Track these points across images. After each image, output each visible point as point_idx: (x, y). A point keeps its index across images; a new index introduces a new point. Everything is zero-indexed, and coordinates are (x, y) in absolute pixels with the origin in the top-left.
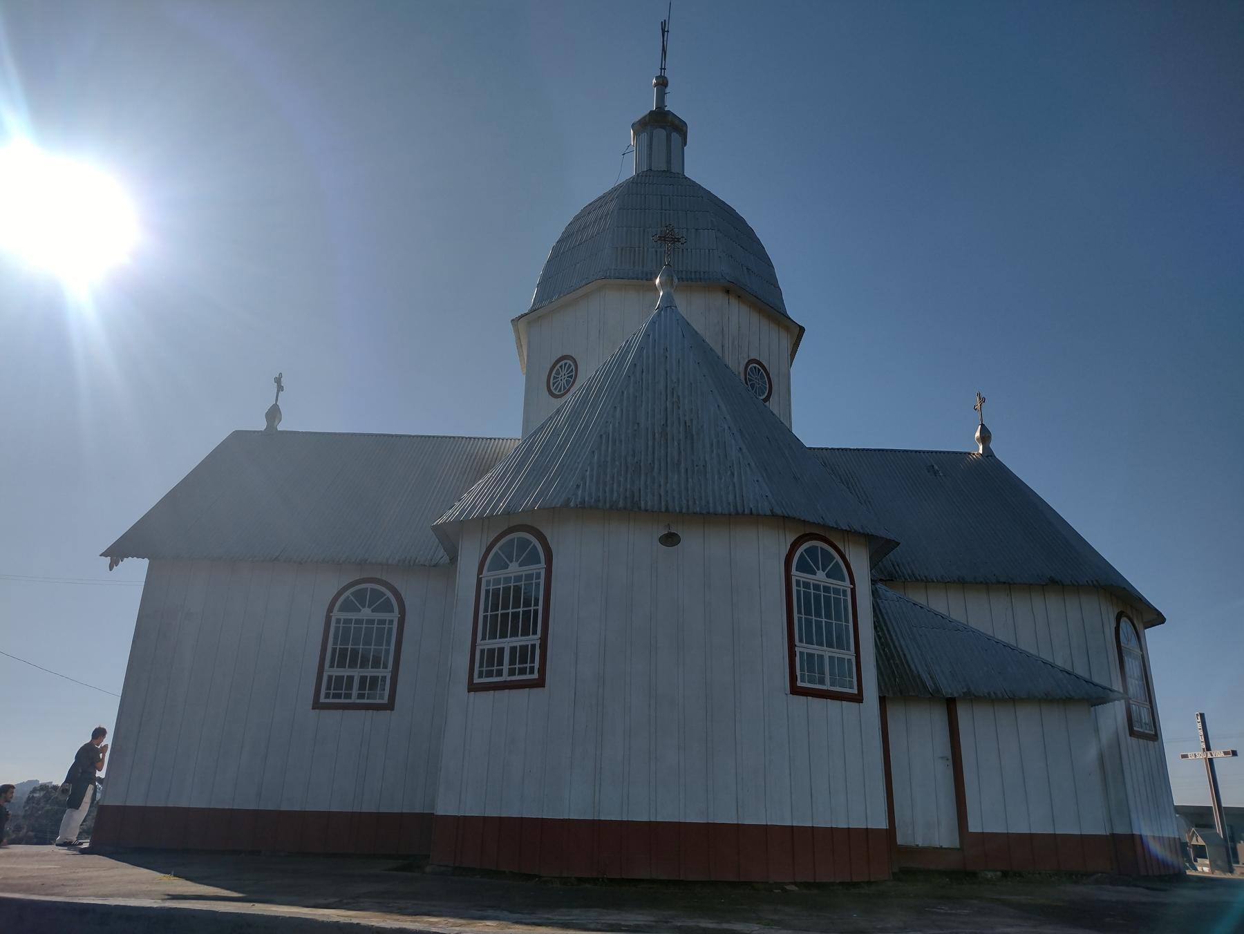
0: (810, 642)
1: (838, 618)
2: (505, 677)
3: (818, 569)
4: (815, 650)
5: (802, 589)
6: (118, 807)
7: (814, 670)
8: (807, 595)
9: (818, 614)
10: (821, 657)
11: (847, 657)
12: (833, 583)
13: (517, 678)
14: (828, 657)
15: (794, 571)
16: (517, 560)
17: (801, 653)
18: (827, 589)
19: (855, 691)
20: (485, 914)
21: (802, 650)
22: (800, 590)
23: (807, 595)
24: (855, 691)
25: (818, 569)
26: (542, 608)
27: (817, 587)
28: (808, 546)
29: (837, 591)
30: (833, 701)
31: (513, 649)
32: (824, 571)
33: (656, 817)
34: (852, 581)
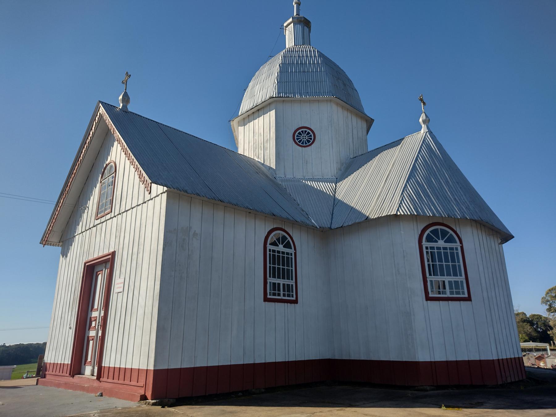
0: (274, 277)
1: (288, 266)
2: (281, 297)
3: (280, 244)
4: (276, 281)
5: (272, 253)
6: (318, 360)
7: (460, 288)
8: (274, 256)
9: (448, 266)
10: (279, 284)
11: (291, 284)
12: (286, 250)
13: (455, 296)
14: (447, 282)
15: (268, 245)
16: (280, 244)
17: (431, 281)
18: (283, 253)
19: (466, 295)
20: (358, 404)
21: (270, 281)
22: (271, 254)
23: (274, 256)
24: (466, 295)
25: (280, 244)
26: (267, 265)
27: (279, 252)
28: (275, 233)
29: (288, 254)
30: (452, 302)
31: (284, 285)
32: (282, 244)
33: (181, 366)
34: (295, 249)
